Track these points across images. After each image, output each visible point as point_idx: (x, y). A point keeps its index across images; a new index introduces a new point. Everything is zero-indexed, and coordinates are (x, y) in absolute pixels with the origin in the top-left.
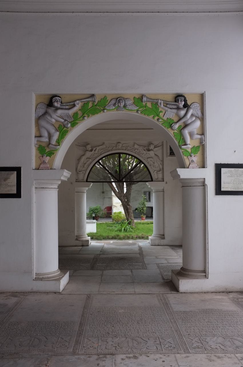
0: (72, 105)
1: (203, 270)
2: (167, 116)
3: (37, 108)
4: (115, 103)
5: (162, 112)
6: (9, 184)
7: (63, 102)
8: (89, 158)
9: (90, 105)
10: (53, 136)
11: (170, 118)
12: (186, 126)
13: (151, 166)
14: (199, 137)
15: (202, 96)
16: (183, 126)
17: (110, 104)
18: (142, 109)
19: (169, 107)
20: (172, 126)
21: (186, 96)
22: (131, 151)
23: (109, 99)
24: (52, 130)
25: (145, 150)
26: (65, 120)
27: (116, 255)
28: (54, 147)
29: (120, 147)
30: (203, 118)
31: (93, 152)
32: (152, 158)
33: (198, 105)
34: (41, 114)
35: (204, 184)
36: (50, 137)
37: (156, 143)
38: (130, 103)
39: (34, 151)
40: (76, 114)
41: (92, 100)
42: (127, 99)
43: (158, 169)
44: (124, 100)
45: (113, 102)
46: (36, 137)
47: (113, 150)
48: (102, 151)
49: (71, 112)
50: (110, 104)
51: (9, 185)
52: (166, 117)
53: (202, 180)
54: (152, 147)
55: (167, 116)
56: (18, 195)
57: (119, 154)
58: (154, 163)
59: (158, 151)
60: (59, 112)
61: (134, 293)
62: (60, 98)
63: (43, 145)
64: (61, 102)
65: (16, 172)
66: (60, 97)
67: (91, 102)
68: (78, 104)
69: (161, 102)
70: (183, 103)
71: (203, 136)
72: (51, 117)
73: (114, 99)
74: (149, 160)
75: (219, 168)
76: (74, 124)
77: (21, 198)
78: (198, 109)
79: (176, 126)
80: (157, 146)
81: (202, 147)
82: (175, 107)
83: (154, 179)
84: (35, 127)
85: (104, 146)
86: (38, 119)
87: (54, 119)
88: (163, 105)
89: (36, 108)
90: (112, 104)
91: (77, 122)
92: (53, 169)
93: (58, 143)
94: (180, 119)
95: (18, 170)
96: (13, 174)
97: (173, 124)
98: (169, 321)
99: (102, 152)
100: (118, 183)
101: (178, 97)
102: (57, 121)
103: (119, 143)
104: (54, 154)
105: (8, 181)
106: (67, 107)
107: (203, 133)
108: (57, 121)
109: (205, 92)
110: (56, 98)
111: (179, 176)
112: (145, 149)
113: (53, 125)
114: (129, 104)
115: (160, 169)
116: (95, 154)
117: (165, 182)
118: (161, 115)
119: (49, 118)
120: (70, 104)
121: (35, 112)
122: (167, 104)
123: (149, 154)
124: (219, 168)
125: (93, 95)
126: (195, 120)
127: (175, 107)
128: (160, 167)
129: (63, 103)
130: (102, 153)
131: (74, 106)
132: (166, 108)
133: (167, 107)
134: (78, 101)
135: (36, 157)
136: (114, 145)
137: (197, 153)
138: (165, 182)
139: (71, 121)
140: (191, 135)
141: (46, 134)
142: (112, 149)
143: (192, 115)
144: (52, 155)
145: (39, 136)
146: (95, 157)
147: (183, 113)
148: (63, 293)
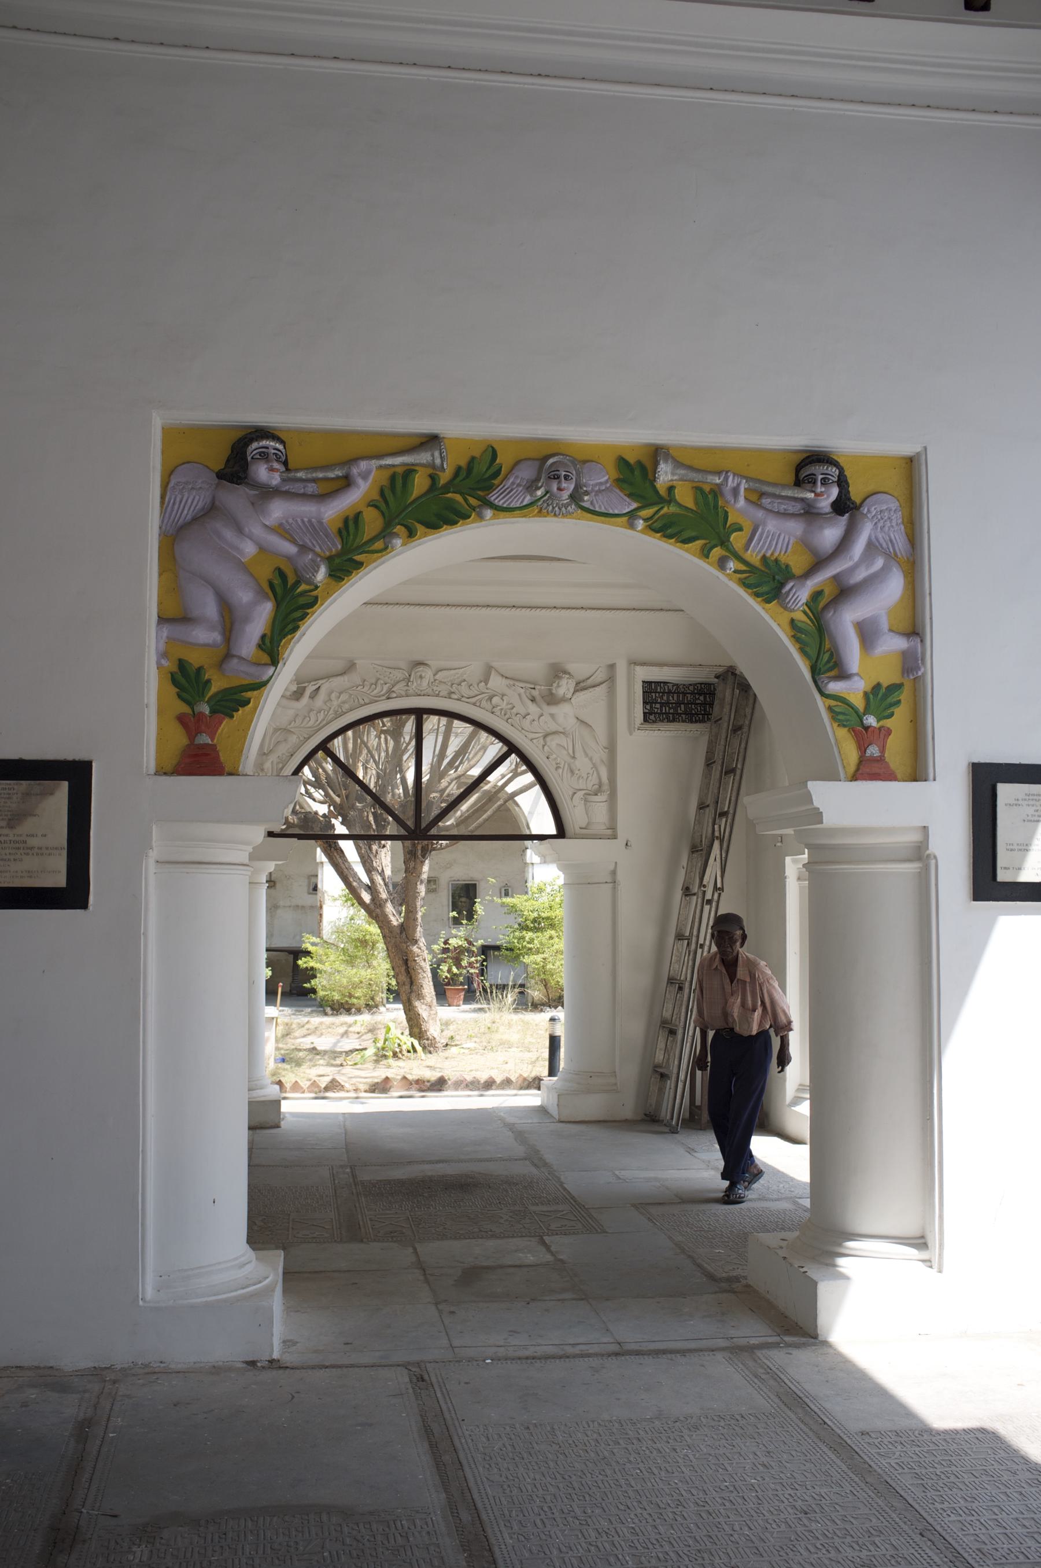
0: (338, 478)
1: (918, 1234)
2: (763, 546)
3: (171, 484)
4: (534, 478)
5: (740, 529)
6: (33, 842)
7: (290, 466)
8: (287, 731)
9: (420, 484)
10: (247, 619)
11: (772, 554)
12: (844, 592)
13: (560, 771)
14: (900, 643)
15: (911, 468)
16: (829, 593)
17: (511, 481)
18: (656, 509)
19: (769, 507)
20: (784, 591)
21: (841, 461)
22: (474, 704)
23: (504, 459)
24: (243, 595)
25: (533, 700)
26: (304, 548)
27: (428, 1170)
28: (252, 670)
29: (425, 683)
30: (914, 562)
31: (305, 699)
32: (563, 733)
33: (894, 505)
34: (187, 514)
35: (920, 853)
36: (232, 624)
37: (580, 669)
38: (601, 484)
39: (152, 684)
40: (351, 523)
41: (430, 458)
42: (585, 462)
43: (591, 783)
44: (575, 466)
45: (526, 473)
46: (162, 620)
47: (394, 695)
48: (344, 697)
49: (333, 511)
50: (511, 481)
51: (32, 848)
52: (760, 551)
53: (915, 837)
54: (565, 687)
55: (763, 546)
56: (73, 894)
57: (420, 714)
58: (574, 757)
59: (591, 704)
60: (278, 510)
61: (614, 1348)
62: (281, 447)
63: (195, 659)
64: (285, 463)
65: (66, 783)
66: (283, 442)
67: (423, 469)
68: (365, 476)
69: (739, 485)
70: (834, 492)
71: (919, 640)
72: (240, 530)
73: (529, 463)
74: (553, 742)
75: (986, 781)
76: (343, 568)
77: (974, 900)
78: (894, 524)
79: (803, 594)
80: (589, 682)
81: (904, 692)
82: (796, 508)
83: (569, 828)
84: (160, 575)
85: (354, 678)
86: (173, 538)
87: (251, 539)
88: (746, 498)
89: (168, 483)
90: (519, 485)
91: (358, 558)
92: (246, 775)
93: (271, 650)
94: (819, 563)
95: (77, 775)
96: (52, 794)
97: (791, 584)
98: (863, 1485)
99: (344, 702)
100: (408, 843)
101: (809, 466)
102: (262, 549)
103: (421, 668)
104: (247, 702)
105: (28, 826)
106: (311, 488)
107: (915, 629)
108: (262, 549)
109: (925, 448)
110: (264, 443)
111: (817, 816)
112: (535, 693)
113: (244, 568)
114: (597, 488)
115: (600, 785)
116: (311, 710)
117: (620, 841)
118: (737, 540)
119: (229, 534)
120: (331, 475)
121: (162, 502)
122: (762, 494)
123: (552, 716)
124: (986, 781)
125: (432, 440)
126: (882, 569)
127: (796, 508)
128: (598, 774)
129: (297, 470)
130: (346, 706)
131: (347, 482)
132: (760, 514)
133: (760, 506)
134: (363, 465)
135: (160, 712)
136: (399, 675)
137: (892, 715)
138: (620, 841)
139: (328, 554)
140: (867, 633)
141: (210, 609)
142: (390, 691)
143: (872, 547)
144: (238, 710)
145: (175, 616)
146: (311, 723)
147: (830, 534)
148: (289, 1359)
